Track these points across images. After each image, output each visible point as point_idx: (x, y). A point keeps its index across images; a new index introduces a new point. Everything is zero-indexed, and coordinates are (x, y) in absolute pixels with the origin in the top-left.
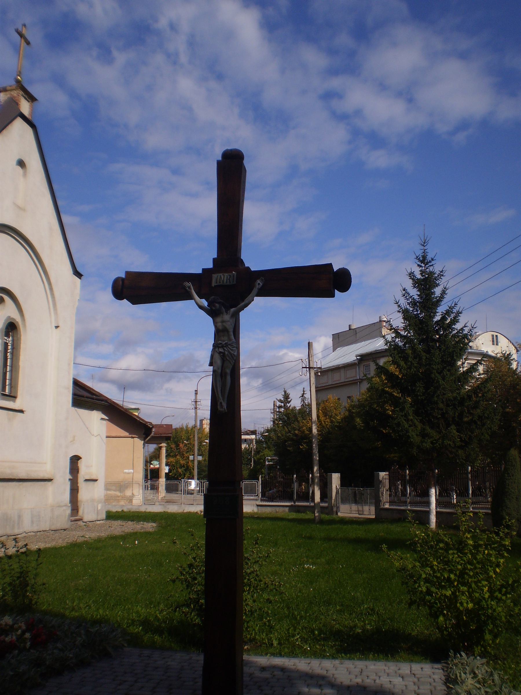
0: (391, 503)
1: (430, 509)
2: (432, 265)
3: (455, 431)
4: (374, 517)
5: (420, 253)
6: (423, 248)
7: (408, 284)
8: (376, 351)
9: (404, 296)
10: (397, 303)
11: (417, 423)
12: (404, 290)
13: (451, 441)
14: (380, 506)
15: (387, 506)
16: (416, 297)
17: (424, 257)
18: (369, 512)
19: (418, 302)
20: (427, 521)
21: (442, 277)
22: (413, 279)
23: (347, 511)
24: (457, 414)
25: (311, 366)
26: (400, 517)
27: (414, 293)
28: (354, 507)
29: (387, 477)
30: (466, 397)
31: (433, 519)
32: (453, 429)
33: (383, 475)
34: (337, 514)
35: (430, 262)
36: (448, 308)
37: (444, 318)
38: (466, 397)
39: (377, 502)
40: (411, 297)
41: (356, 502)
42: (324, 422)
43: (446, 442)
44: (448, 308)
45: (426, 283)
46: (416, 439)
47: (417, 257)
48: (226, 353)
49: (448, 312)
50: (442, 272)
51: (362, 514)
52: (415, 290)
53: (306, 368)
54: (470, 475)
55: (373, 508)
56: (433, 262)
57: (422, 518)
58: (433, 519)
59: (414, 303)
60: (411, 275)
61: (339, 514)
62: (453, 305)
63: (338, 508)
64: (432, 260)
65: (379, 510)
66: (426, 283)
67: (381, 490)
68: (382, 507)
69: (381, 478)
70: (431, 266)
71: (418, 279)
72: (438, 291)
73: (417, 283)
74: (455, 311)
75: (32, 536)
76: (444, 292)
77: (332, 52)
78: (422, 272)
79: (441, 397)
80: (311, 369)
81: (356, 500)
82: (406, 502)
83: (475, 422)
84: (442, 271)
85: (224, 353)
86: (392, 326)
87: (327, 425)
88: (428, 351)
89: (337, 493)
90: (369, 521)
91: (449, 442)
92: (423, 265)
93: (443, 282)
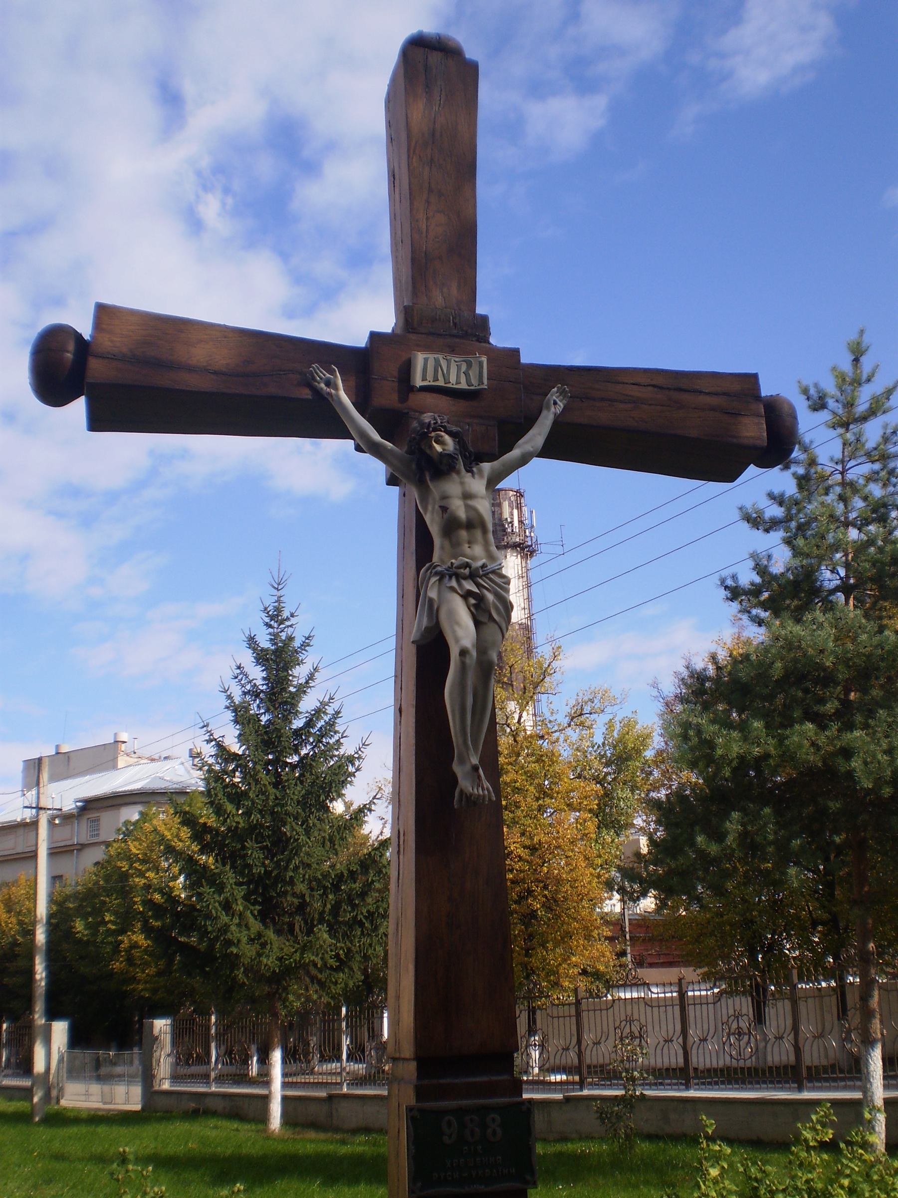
0: (175, 1078)
1: (270, 1092)
2: (291, 626)
3: (326, 936)
4: (138, 1107)
5: (270, 602)
6: (275, 592)
7: (247, 658)
8: (113, 793)
9: (236, 678)
10: (226, 691)
11: (251, 920)
12: (239, 667)
13: (317, 955)
14: (152, 1086)
15: (166, 1086)
16: (259, 682)
17: (278, 610)
18: (128, 1097)
19: (262, 691)
20: (263, 1117)
21: (307, 648)
22: (254, 649)
23: (79, 1096)
24: (329, 906)
25: (42, 805)
26: (198, 1109)
27: (257, 674)
28: (95, 1088)
29: (168, 1029)
30: (346, 873)
31: (276, 1109)
32: (323, 934)
33: (161, 1025)
34: (58, 1102)
35: (288, 619)
36: (318, 705)
37: (310, 724)
38: (346, 873)
39: (148, 1077)
40: (250, 682)
41: (99, 1079)
42: (6, 922)
43: (309, 957)
44: (318, 705)
45: (278, 659)
46: (248, 951)
47: (266, 609)
48: (490, 597)
49: (319, 712)
50: (307, 639)
51: (110, 1103)
52: (259, 668)
53: (31, 808)
54: (344, 1024)
55: (137, 1091)
56: (293, 621)
57: (253, 1111)
58: (276, 1109)
59: (255, 693)
60: (252, 642)
61: (63, 1102)
62: (326, 700)
63: (61, 1090)
64: (292, 615)
65: (150, 1094)
66: (278, 659)
67: (156, 1055)
68: (156, 1088)
69: (156, 1032)
70: (288, 626)
71: (263, 650)
72: (299, 673)
73: (262, 657)
74: (330, 710)
75: (624, 986)
76: (311, 677)
77: (298, 278)
78: (274, 639)
79: (301, 871)
80: (42, 812)
81: (99, 1073)
82: (207, 1076)
83: (361, 924)
84: (309, 637)
85: (480, 598)
86: (212, 735)
87: (11, 929)
88: (278, 783)
89: (61, 1060)
90: (126, 1118)
91: (312, 958)
92: (276, 625)
93: (309, 660)
